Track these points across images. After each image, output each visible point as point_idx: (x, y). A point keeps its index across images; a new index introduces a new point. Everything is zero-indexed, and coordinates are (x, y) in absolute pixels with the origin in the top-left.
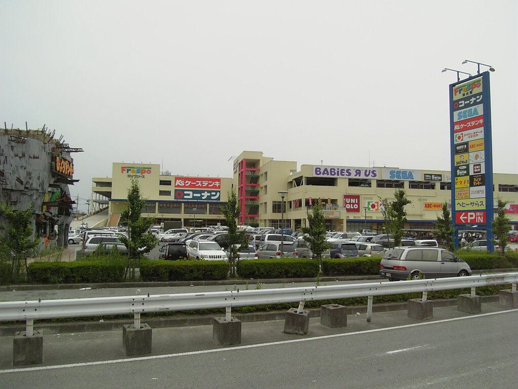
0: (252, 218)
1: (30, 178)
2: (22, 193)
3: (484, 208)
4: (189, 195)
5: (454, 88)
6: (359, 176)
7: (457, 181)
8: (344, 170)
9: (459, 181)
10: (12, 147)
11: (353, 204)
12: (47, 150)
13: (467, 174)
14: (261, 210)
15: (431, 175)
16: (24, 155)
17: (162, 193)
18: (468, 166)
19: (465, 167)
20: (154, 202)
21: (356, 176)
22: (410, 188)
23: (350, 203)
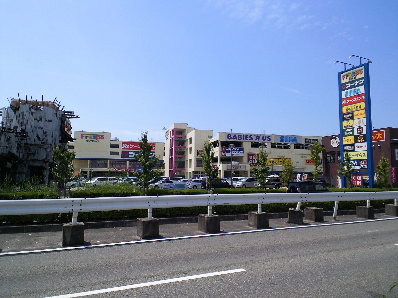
0: (179, 171)
1: (46, 136)
2: (39, 147)
3: (366, 158)
4: (132, 155)
5: (342, 75)
6: (259, 140)
7: (345, 140)
8: (248, 136)
9: (346, 139)
10: (32, 114)
11: (361, 131)
12: (58, 115)
13: (353, 134)
14: (187, 164)
15: (310, 139)
16: (41, 119)
17: (112, 153)
18: (353, 129)
19: (351, 130)
20: (108, 159)
21: (256, 140)
22: (294, 149)
23: (252, 160)
